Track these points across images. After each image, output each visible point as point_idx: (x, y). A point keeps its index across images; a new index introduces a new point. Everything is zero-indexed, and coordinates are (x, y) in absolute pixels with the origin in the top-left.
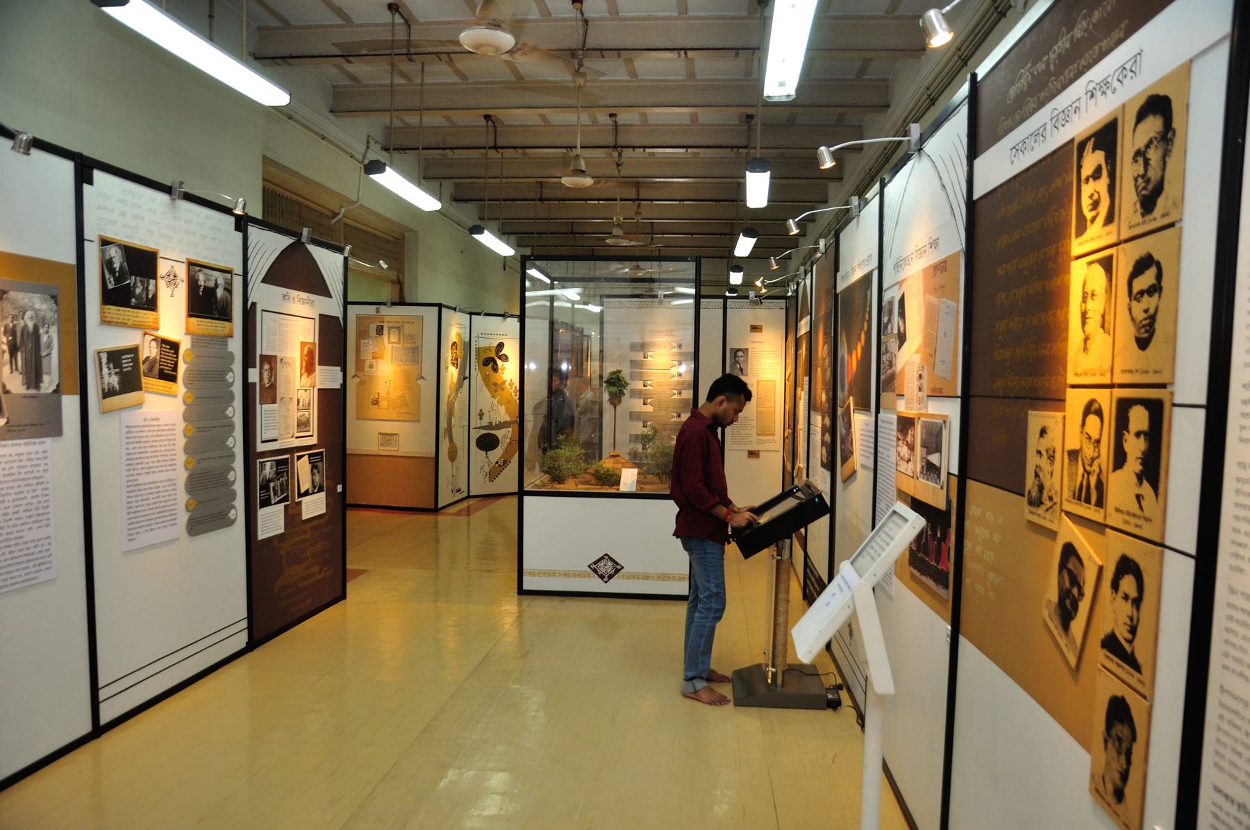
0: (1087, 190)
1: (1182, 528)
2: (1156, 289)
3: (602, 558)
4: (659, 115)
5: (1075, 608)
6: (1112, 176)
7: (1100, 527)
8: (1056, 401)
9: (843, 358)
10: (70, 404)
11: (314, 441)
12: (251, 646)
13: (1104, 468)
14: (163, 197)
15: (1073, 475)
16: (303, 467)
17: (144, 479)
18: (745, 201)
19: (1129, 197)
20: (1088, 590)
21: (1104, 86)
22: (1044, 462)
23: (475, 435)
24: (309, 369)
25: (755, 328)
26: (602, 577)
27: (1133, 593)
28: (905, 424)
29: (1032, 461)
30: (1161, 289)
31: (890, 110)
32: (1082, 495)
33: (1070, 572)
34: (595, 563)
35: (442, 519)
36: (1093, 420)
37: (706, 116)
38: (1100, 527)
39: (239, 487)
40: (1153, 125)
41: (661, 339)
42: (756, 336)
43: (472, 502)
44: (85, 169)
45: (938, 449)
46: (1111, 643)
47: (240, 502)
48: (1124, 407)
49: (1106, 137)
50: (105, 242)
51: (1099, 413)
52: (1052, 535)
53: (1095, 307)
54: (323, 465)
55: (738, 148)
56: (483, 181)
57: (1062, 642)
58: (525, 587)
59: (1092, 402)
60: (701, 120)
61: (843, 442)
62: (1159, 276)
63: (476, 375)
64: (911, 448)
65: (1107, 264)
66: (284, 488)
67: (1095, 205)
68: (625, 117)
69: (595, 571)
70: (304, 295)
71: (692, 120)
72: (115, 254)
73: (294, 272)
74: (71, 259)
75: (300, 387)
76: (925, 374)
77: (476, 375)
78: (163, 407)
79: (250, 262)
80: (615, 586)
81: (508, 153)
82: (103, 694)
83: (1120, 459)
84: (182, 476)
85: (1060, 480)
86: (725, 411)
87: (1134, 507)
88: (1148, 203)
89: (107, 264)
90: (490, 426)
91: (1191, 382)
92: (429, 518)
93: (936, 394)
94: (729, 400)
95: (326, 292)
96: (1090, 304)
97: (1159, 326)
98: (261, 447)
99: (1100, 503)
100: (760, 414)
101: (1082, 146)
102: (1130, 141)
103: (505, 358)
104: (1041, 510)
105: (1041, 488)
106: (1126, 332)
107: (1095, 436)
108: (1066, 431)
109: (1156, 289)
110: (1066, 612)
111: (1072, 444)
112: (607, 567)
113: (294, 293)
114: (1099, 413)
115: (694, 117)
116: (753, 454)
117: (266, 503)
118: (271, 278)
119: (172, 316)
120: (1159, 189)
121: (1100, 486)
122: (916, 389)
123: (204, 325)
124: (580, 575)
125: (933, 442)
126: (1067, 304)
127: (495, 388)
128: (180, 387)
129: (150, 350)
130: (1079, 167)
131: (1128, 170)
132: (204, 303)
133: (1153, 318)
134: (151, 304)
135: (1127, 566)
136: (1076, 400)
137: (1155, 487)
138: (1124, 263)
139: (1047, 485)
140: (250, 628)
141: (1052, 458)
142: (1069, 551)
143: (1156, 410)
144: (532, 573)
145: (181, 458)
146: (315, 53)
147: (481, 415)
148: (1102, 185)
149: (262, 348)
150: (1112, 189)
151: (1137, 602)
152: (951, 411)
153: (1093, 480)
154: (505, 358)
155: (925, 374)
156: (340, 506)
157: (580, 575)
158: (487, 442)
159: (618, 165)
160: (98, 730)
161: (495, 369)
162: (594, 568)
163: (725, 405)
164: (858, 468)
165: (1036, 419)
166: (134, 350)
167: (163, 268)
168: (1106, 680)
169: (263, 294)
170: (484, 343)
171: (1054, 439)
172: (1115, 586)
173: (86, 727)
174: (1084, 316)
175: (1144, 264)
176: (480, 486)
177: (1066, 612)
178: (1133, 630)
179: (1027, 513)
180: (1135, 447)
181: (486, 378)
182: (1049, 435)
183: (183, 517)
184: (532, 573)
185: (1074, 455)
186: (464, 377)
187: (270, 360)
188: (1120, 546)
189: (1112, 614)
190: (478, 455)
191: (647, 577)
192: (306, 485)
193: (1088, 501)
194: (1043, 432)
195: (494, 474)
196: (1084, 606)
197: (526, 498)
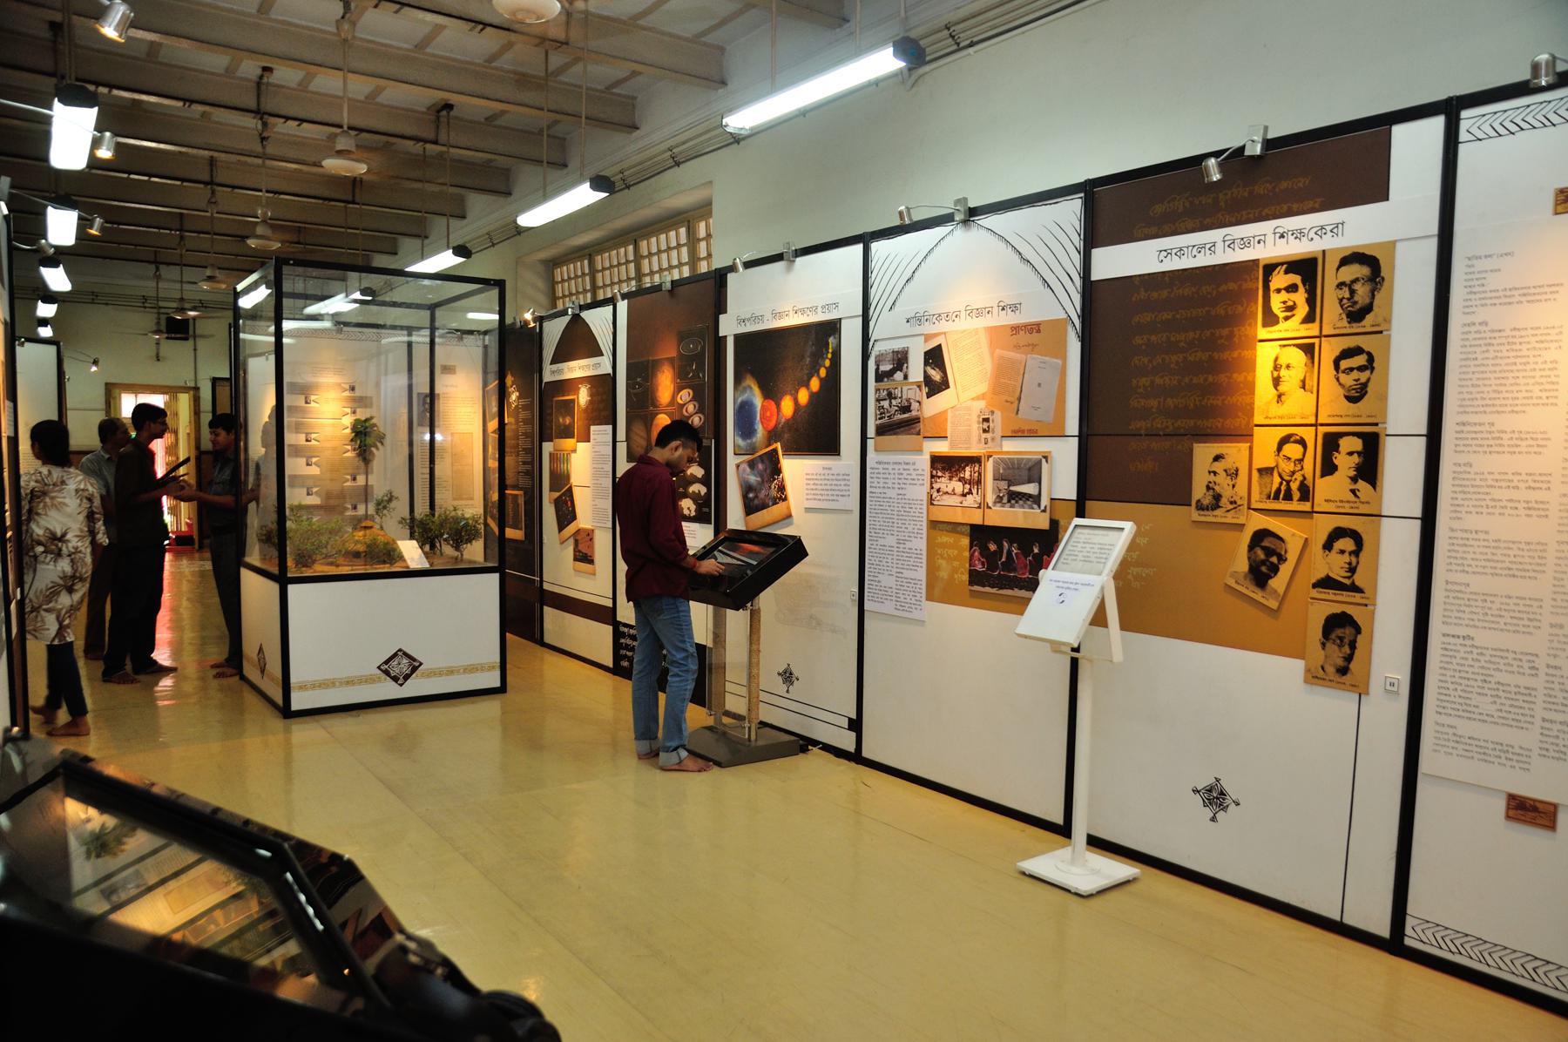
3: (395, 655)
4: (327, 82)
8: (1247, 436)
9: (745, 411)
13: (1309, 476)
18: (46, 160)
20: (1292, 557)
22: (1222, 479)
26: (395, 679)
28: (945, 465)
30: (1373, 369)
31: (637, 134)
34: (386, 662)
48: (1331, 443)
49: (1306, 269)
51: (1302, 442)
55: (426, 141)
56: (419, 185)
58: (498, 684)
60: (383, 98)
65: (1308, 350)
68: (285, 75)
69: (387, 673)
71: (148, 54)
79: (872, 324)
80: (413, 688)
86: (680, 457)
88: (1357, 314)
94: (684, 446)
101: (1270, 269)
104: (1217, 512)
105: (1217, 497)
110: (1261, 574)
111: (1269, 462)
114: (1302, 442)
124: (369, 680)
136: (1265, 441)
138: (1329, 350)
144: (303, 687)
146: (1413, 243)
148: (1300, 297)
150: (1311, 301)
157: (369, 680)
159: (263, 139)
162: (385, 669)
163: (680, 451)
165: (1203, 453)
172: (1328, 546)
174: (1276, 382)
177: (1261, 574)
184: (303, 687)
191: (451, 672)
197: (291, 588)
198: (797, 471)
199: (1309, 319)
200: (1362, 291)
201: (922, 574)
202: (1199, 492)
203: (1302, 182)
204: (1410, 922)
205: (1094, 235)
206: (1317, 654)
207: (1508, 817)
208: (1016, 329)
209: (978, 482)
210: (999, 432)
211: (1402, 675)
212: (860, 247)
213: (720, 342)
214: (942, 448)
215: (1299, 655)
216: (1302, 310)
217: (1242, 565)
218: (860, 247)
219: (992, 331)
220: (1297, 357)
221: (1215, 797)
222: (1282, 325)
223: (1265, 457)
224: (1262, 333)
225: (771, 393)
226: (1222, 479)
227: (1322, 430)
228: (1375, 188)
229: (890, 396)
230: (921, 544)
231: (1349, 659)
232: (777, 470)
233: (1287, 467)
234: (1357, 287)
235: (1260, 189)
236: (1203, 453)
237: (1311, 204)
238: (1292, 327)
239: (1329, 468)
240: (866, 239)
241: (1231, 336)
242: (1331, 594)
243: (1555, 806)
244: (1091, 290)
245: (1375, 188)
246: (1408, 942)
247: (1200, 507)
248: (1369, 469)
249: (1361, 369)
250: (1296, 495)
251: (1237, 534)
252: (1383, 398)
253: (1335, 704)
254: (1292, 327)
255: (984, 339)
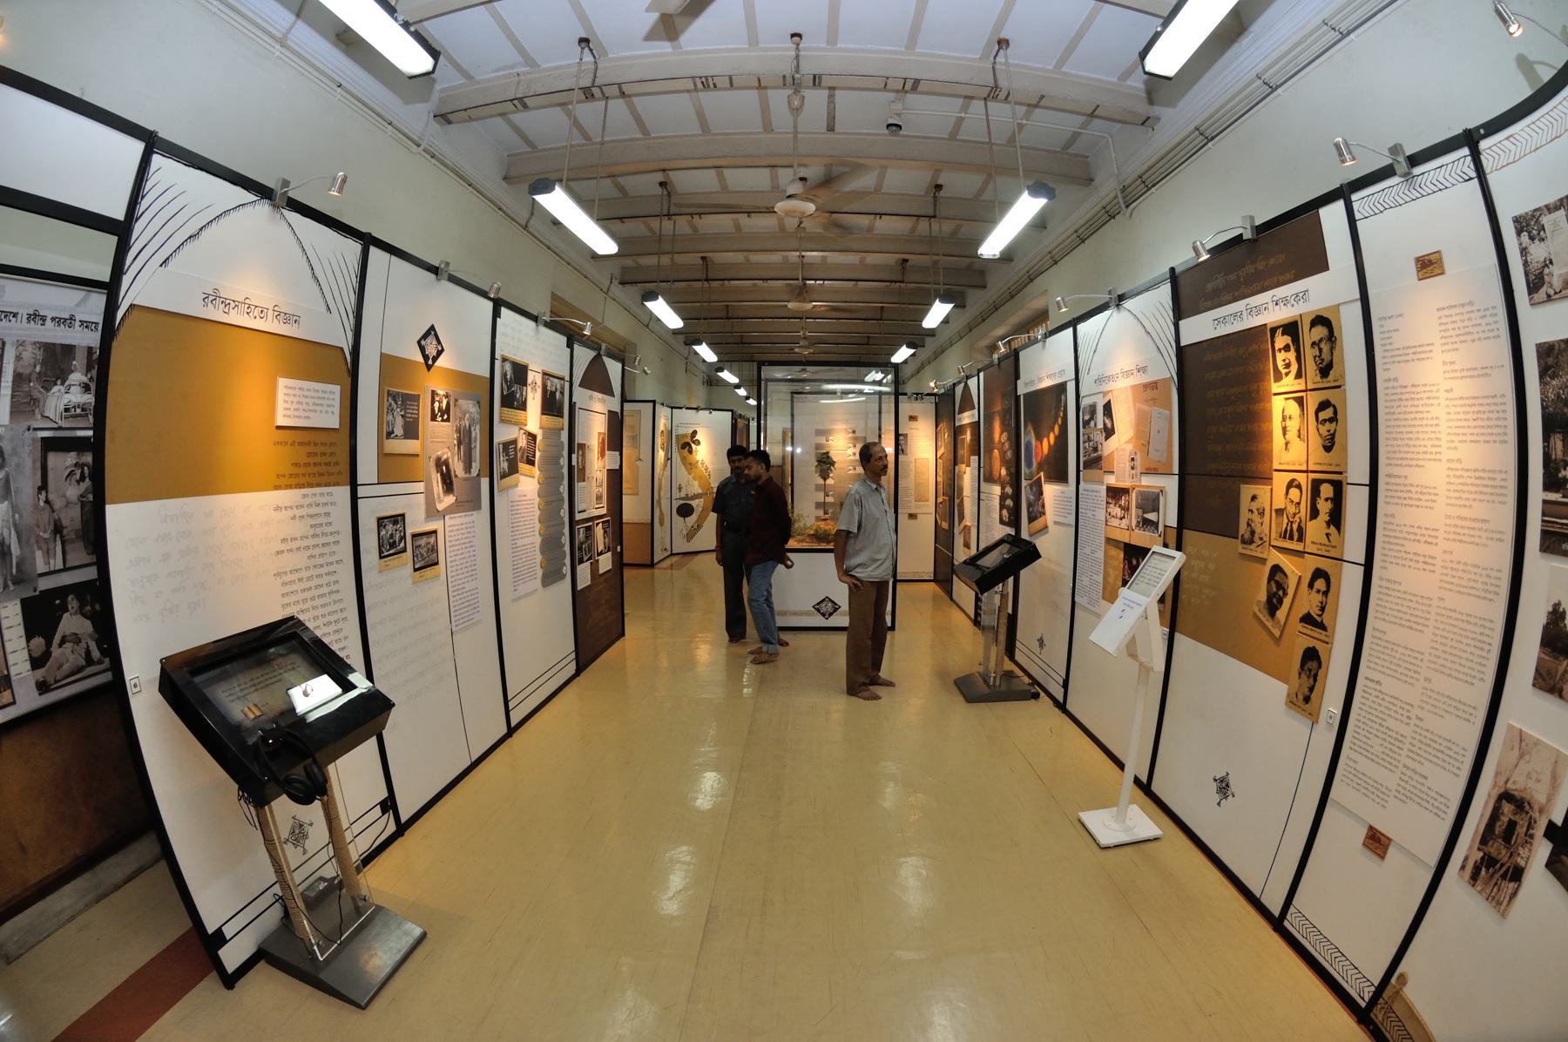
0: (1280, 357)
1: (1354, 546)
2: (1333, 419)
5: (1281, 602)
6: (1298, 351)
7: (1300, 554)
8: (1267, 479)
9: (1028, 445)
10: (485, 482)
11: (604, 511)
12: (578, 673)
14: (532, 324)
15: (1279, 525)
16: (599, 531)
17: (520, 543)
19: (1311, 368)
20: (1291, 591)
21: (1285, 301)
22: (1255, 516)
23: (676, 505)
24: (602, 454)
25: (912, 418)
27: (1324, 588)
28: (1115, 493)
29: (1244, 516)
32: (1287, 535)
33: (1277, 582)
35: (656, 572)
36: (1294, 492)
37: (872, 259)
38: (1300, 554)
39: (567, 548)
40: (1320, 332)
41: (840, 426)
42: (914, 424)
43: (674, 559)
44: (498, 304)
45: (1156, 509)
46: (1307, 619)
47: (568, 561)
48: (1316, 486)
49: (1291, 329)
50: (504, 360)
51: (1299, 487)
52: (1263, 561)
53: (1293, 426)
54: (610, 530)
57: (1269, 624)
59: (1293, 481)
61: (1030, 505)
62: (1335, 412)
63: (676, 456)
64: (1126, 509)
65: (1300, 401)
66: (590, 549)
67: (1288, 366)
70: (600, 395)
72: (508, 367)
73: (596, 379)
74: (487, 375)
75: (598, 466)
76: (1138, 458)
77: (676, 456)
78: (527, 485)
81: (715, 284)
82: (511, 705)
83: (1314, 513)
84: (538, 540)
85: (1268, 527)
87: (1325, 540)
88: (1325, 371)
89: (504, 375)
90: (687, 498)
91: (1358, 470)
92: (647, 571)
93: (1150, 471)
95: (610, 392)
96: (1288, 423)
97: (1337, 439)
98: (578, 517)
99: (1300, 539)
100: (917, 485)
101: (1273, 331)
102: (1310, 336)
103: (698, 443)
104: (1253, 546)
105: (1253, 533)
106: (1316, 442)
107: (1296, 500)
108: (1275, 496)
109: (1333, 419)
110: (1273, 605)
111: (1279, 504)
112: (829, 607)
113: (596, 394)
114: (1299, 487)
115: (862, 261)
116: (912, 516)
117: (581, 561)
118: (585, 384)
119: (533, 418)
120: (1330, 366)
121: (1300, 529)
122: (1128, 468)
123: (550, 421)
124: (807, 614)
125: (1151, 502)
126: (1271, 420)
127: (690, 466)
128: (536, 471)
129: (522, 442)
130: (1273, 343)
131: (1309, 353)
132: (551, 405)
133: (1333, 435)
134: (523, 406)
135: (1319, 574)
136: (1280, 480)
137: (1339, 530)
138: (1312, 401)
139: (1258, 531)
140: (577, 658)
141: (1262, 513)
142: (1276, 569)
143: (1338, 487)
145: (538, 526)
147: (680, 489)
148: (1292, 355)
149: (578, 439)
150: (1298, 359)
151: (1326, 593)
152: (1171, 485)
153: (1295, 527)
154: (698, 443)
155: (1138, 458)
156: (620, 564)
157: (807, 614)
158: (685, 511)
160: (511, 731)
161: (690, 452)
164: (1050, 524)
165: (1247, 491)
166: (514, 442)
167: (531, 377)
168: (1302, 639)
169: (581, 395)
170: (682, 431)
171: (1264, 501)
172: (1311, 586)
173: (505, 730)
174: (1284, 430)
175: (1324, 405)
176: (681, 546)
177: (1273, 605)
178: (1323, 609)
179: (1240, 548)
180: (1324, 507)
181: (683, 459)
182: (1259, 500)
183: (540, 572)
185: (1280, 512)
186: (669, 459)
187: (582, 447)
188: (1312, 563)
189: (1309, 602)
190: (678, 520)
192: (601, 548)
193: (1291, 538)
194: (1254, 498)
195: (690, 535)
196: (1287, 601)
198: (1050, 491)
199: (1299, 375)
200: (1325, 347)
201: (1100, 578)
202: (1243, 528)
203: (1281, 258)
204: (1292, 909)
205: (1180, 310)
206: (1295, 681)
207: (1364, 844)
208: (1146, 386)
209: (1126, 509)
210: (1139, 469)
211: (1337, 711)
212: (1340, 204)
213: (1017, 398)
214: (1111, 480)
215: (1285, 681)
216: (1294, 368)
217: (1263, 597)
218: (1340, 204)
219: (1134, 387)
220: (1293, 408)
221: (1223, 787)
222: (1286, 380)
223: (1279, 502)
224: (1275, 388)
225: (1039, 438)
226: (1255, 516)
227: (1312, 476)
228: (1316, 262)
229: (1089, 440)
230: (1100, 555)
231: (1311, 689)
232: (1041, 493)
233: (1291, 509)
234: (1322, 345)
235: (1261, 265)
236: (1247, 491)
237: (1288, 276)
238: (1289, 383)
239: (1314, 513)
240: (1074, 323)
241: (1258, 390)
242: (1309, 629)
243: (1390, 840)
244: (1181, 351)
245: (1316, 262)
246: (1286, 923)
247: (1243, 542)
248: (1336, 519)
249: (1331, 420)
250: (1296, 536)
251: (1259, 566)
252: (1345, 449)
253: (1296, 725)
254: (1289, 383)
255: (1129, 393)
